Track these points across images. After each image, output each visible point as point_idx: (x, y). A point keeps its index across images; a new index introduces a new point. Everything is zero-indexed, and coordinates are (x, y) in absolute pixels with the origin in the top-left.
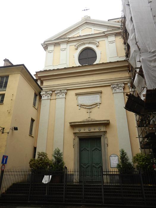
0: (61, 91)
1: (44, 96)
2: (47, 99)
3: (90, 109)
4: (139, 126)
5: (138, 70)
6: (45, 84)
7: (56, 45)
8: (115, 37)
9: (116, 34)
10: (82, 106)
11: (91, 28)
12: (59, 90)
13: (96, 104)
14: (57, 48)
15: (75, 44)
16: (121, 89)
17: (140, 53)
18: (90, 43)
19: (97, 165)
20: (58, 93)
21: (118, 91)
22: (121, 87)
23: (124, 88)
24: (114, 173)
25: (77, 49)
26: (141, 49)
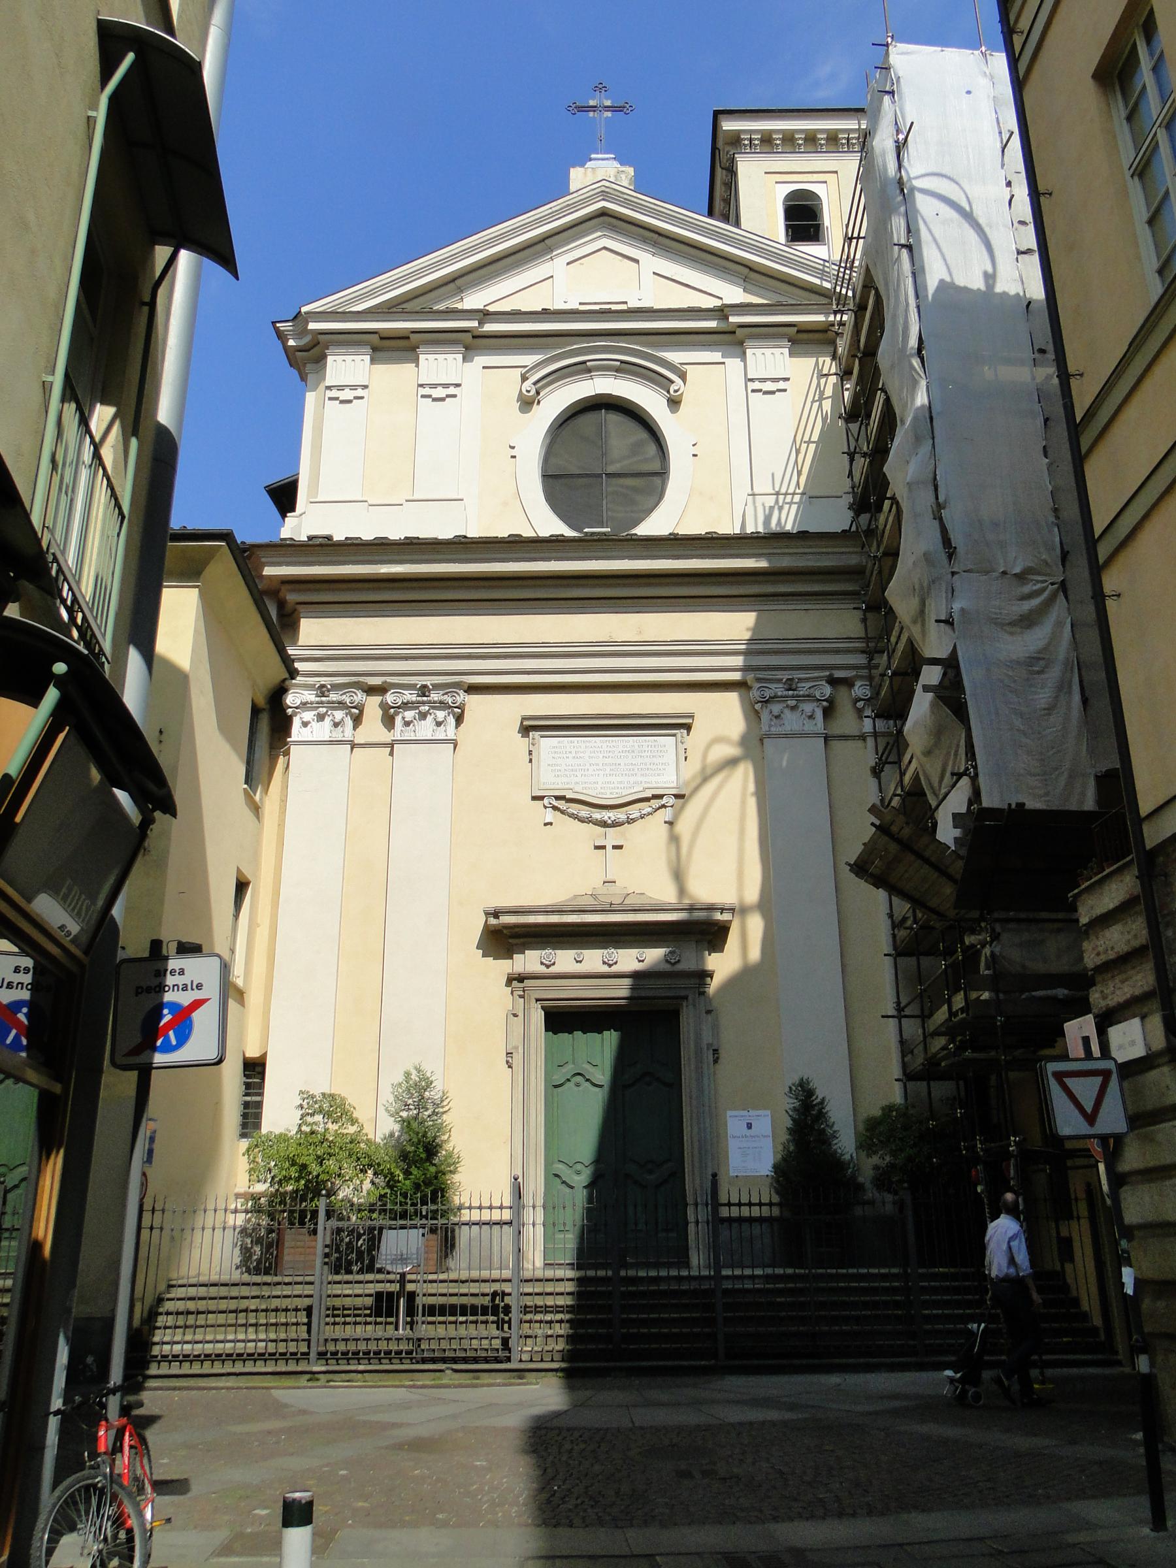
0: (424, 691)
1: (308, 716)
2: (331, 742)
3: (615, 824)
4: (900, 951)
5: (931, 675)
6: (314, 631)
7: (388, 349)
8: (791, 355)
9: (798, 332)
10: (564, 803)
11: (637, 261)
12: (411, 687)
13: (655, 797)
14: (394, 377)
15: (530, 360)
16: (811, 717)
17: (953, 573)
18: (624, 369)
19: (650, 1172)
20: (406, 706)
21: (792, 721)
22: (810, 697)
23: (829, 712)
24: (745, 1212)
25: (527, 403)
26: (961, 550)
